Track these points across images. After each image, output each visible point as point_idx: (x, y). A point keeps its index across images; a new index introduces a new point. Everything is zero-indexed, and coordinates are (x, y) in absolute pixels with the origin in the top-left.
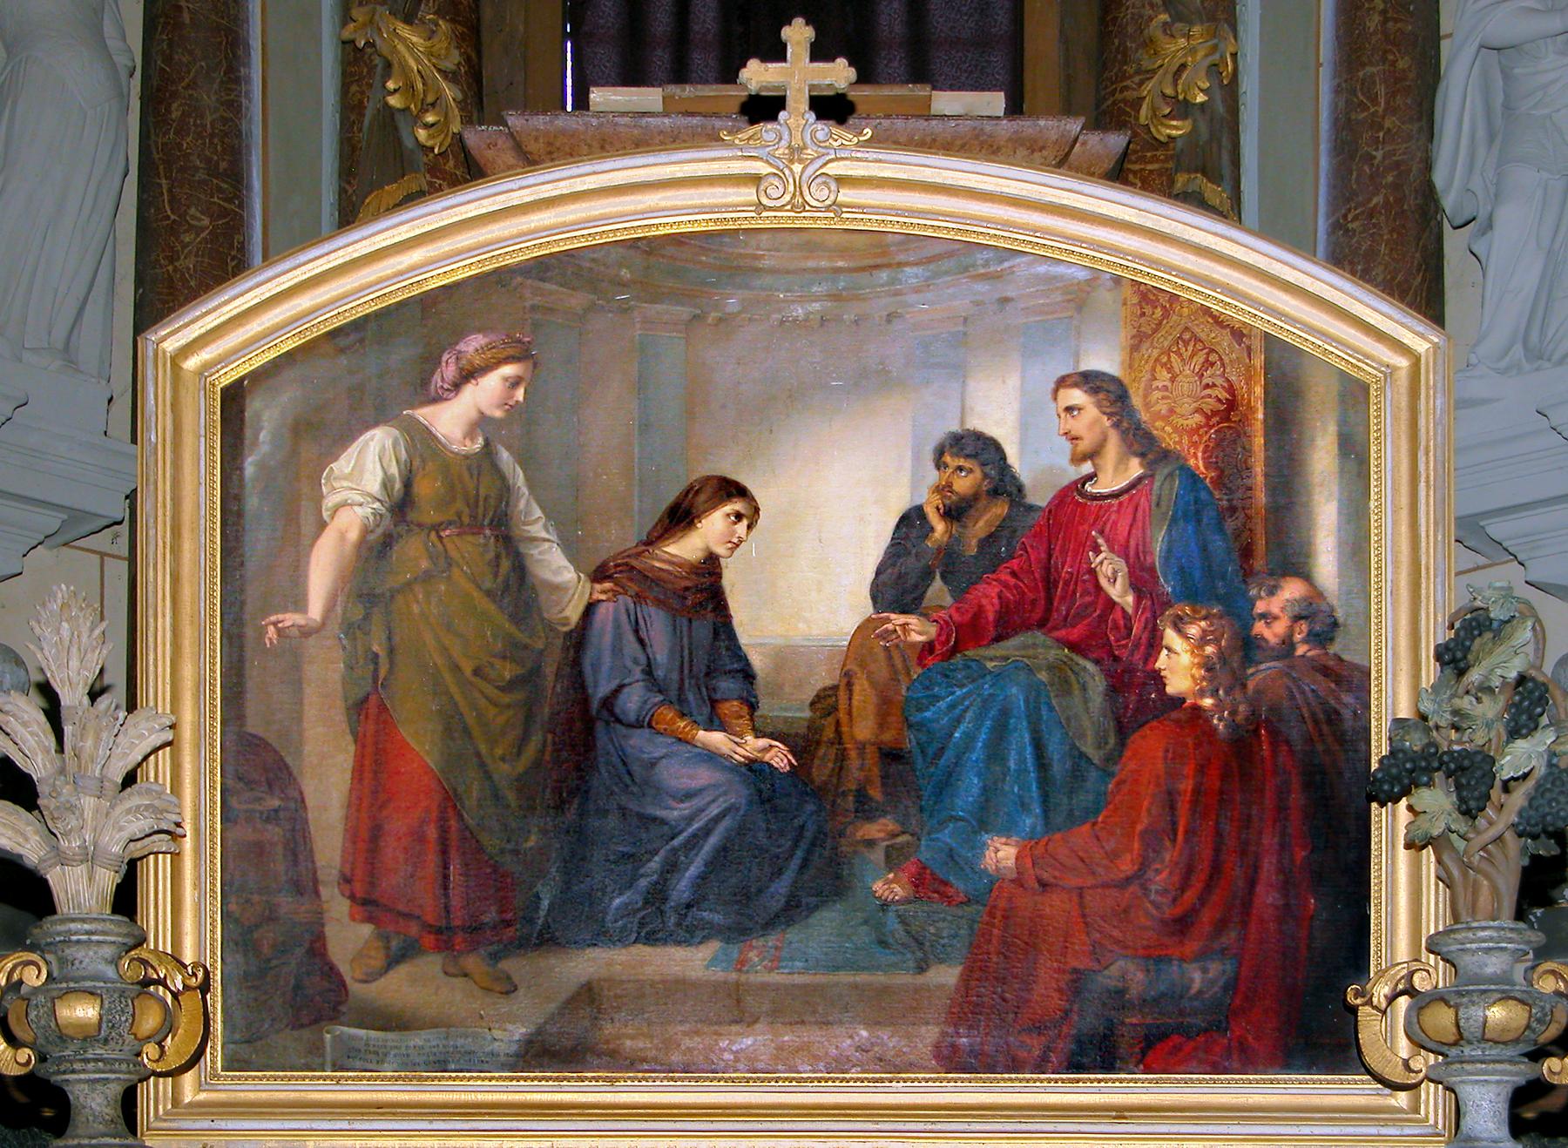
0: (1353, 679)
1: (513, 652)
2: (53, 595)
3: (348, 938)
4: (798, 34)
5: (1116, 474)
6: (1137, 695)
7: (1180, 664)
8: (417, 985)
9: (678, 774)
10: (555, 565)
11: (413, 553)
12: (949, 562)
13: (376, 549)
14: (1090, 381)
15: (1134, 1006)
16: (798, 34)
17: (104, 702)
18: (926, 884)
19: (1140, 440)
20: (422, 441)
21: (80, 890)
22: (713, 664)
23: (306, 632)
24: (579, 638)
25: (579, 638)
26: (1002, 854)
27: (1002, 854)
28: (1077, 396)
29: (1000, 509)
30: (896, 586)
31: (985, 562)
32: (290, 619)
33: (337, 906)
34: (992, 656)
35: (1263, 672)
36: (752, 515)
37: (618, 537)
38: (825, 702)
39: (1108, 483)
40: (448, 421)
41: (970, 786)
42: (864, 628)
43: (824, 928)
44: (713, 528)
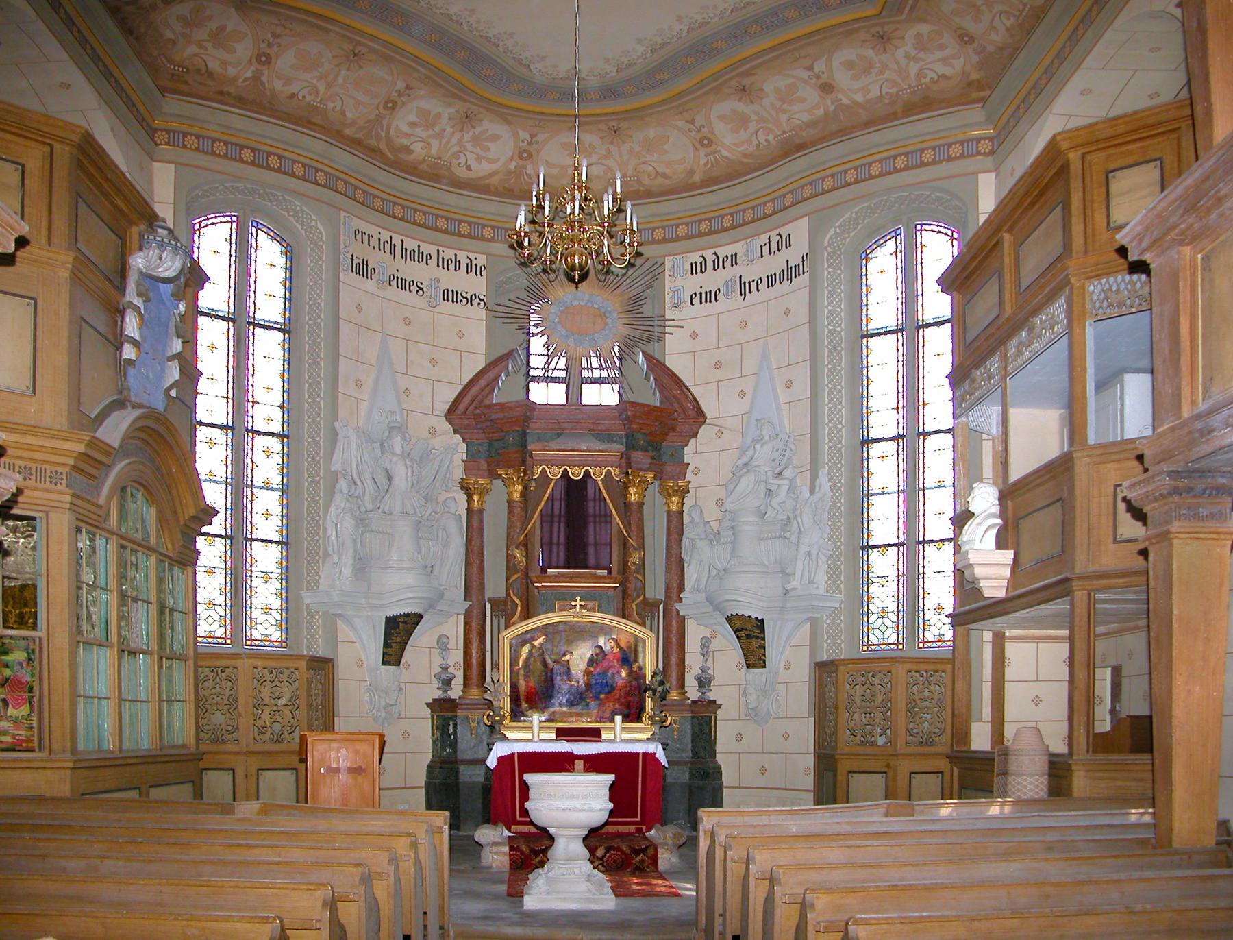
5: (616, 650)
13: (527, 660)
44: (567, 658)
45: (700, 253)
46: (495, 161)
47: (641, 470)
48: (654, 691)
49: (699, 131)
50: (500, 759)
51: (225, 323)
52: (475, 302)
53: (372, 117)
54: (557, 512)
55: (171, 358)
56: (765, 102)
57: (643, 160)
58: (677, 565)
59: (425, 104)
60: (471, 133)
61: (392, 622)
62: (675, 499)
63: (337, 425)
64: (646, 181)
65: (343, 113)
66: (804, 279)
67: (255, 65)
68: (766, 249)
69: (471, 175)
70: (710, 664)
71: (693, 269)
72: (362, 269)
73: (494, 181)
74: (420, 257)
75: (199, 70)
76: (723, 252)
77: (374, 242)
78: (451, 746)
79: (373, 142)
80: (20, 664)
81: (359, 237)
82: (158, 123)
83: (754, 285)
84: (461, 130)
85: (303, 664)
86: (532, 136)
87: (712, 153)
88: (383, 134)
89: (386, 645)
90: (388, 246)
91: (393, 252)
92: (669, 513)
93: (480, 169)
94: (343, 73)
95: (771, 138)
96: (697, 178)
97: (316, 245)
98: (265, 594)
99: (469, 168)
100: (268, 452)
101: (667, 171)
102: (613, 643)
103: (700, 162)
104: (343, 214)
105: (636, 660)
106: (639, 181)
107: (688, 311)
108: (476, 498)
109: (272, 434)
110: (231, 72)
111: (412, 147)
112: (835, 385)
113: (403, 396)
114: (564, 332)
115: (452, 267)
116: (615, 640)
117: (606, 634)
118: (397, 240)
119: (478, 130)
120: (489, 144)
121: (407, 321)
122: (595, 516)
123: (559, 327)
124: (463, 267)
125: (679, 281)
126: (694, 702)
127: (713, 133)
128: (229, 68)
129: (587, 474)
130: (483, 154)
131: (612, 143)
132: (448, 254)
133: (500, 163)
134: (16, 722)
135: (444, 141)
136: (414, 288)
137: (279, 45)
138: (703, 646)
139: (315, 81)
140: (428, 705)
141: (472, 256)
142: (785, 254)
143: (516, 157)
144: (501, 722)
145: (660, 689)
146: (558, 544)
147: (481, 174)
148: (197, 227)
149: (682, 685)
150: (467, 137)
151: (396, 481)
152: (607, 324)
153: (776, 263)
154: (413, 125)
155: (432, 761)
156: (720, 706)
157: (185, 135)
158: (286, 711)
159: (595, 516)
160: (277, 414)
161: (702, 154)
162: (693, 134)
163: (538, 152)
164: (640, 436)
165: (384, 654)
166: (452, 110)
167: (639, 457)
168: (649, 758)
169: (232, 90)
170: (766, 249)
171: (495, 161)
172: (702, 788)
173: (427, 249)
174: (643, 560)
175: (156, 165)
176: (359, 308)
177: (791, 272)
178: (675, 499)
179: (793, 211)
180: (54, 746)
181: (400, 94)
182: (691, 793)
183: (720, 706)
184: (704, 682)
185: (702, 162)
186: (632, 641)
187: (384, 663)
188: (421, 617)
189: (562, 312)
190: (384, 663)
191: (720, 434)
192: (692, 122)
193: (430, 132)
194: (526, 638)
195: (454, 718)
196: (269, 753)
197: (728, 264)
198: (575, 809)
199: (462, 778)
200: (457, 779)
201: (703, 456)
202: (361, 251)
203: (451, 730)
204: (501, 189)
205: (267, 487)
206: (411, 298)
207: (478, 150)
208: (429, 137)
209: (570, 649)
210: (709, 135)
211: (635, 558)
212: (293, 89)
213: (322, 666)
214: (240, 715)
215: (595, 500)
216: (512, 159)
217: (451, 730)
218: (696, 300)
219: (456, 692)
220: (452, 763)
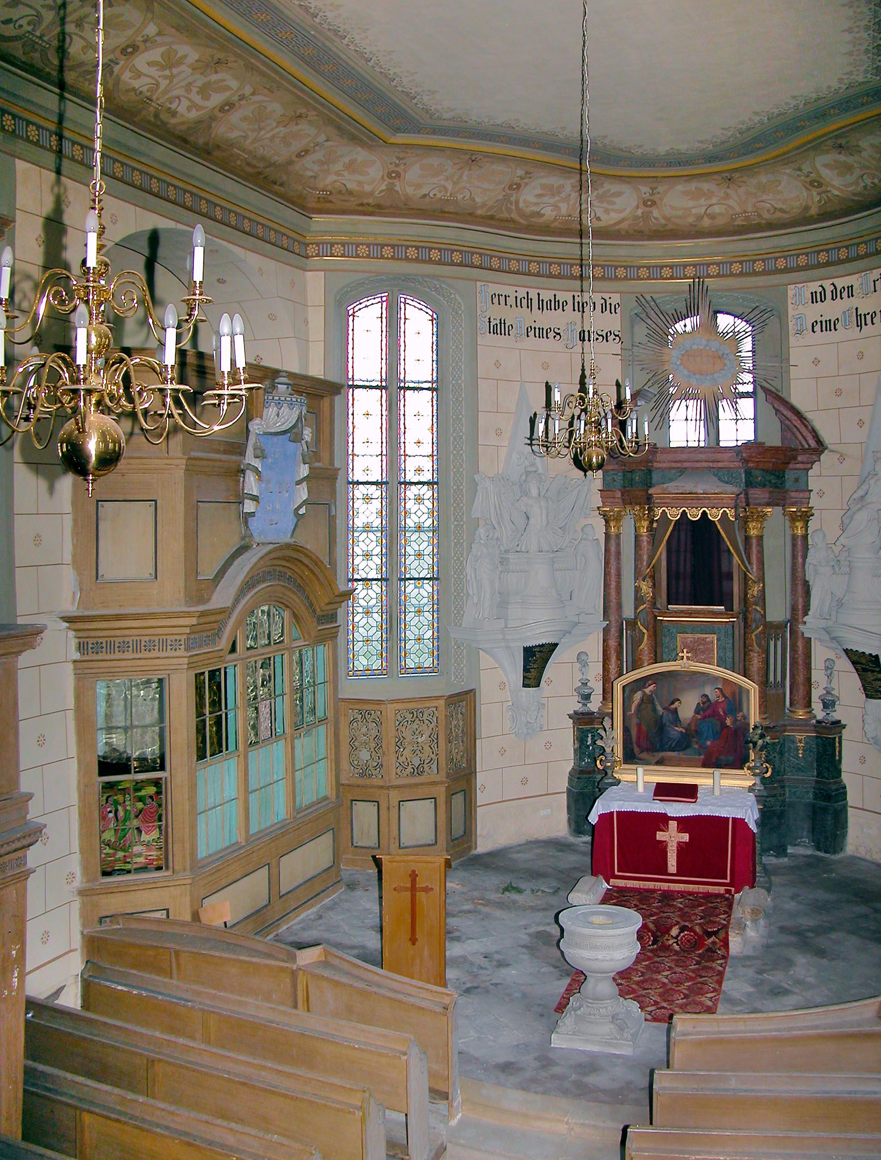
3: (636, 750)
4: (685, 837)
6: (724, 726)
7: (728, 722)
8: (644, 755)
9: (673, 732)
10: (659, 708)
11: (644, 706)
13: (639, 705)
16: (685, 837)
18: (700, 746)
19: (724, 696)
21: (608, 750)
22: (677, 720)
24: (661, 716)
25: (661, 716)
26: (709, 743)
27: (709, 743)
30: (697, 711)
31: (706, 708)
33: (635, 746)
34: (707, 720)
35: (738, 723)
38: (689, 725)
40: (647, 691)
41: (705, 735)
43: (688, 751)
44: (677, 703)
45: (820, 283)
46: (621, 211)
47: (759, 504)
48: (755, 744)
49: (807, 176)
50: (601, 816)
51: (379, 391)
52: (610, 338)
53: (500, 197)
55: (299, 483)
56: (863, 154)
57: (759, 199)
58: (802, 591)
59: (545, 181)
61: (529, 652)
62: (799, 524)
63: (476, 477)
64: (766, 215)
65: (473, 200)
67: (388, 180)
70: (834, 684)
71: (815, 298)
72: (499, 328)
73: (624, 226)
74: (556, 305)
75: (340, 192)
76: (840, 283)
79: (505, 215)
80: (151, 797)
81: (496, 300)
82: (309, 239)
83: (869, 317)
85: (442, 702)
86: (653, 189)
87: (824, 192)
88: (513, 207)
89: (526, 670)
90: (524, 302)
91: (530, 306)
92: (794, 537)
94: (466, 173)
96: (813, 211)
98: (419, 627)
99: (598, 219)
100: (419, 499)
101: (784, 207)
103: (814, 201)
105: (741, 710)
106: (759, 215)
108: (612, 524)
109: (423, 483)
110: (368, 188)
114: (686, 372)
118: (533, 295)
120: (614, 199)
123: (681, 368)
124: (598, 307)
126: (818, 722)
127: (821, 177)
128: (365, 186)
131: (728, 187)
134: (148, 845)
135: (571, 203)
137: (405, 164)
138: (827, 668)
139: (442, 182)
140: (570, 717)
141: (606, 296)
144: (612, 767)
145: (760, 742)
148: (351, 312)
149: (808, 704)
151: (532, 521)
152: (725, 365)
154: (539, 196)
156: (844, 727)
157: (332, 245)
158: (426, 748)
160: (427, 464)
161: (814, 193)
163: (661, 199)
164: (757, 473)
165: (524, 677)
166: (573, 181)
167: (757, 494)
168: (739, 823)
169: (370, 201)
171: (621, 211)
172: (825, 810)
173: (561, 296)
174: (763, 591)
175: (309, 274)
176: (497, 365)
178: (799, 524)
180: (177, 868)
181: (522, 178)
182: (814, 813)
183: (844, 727)
187: (525, 686)
188: (556, 645)
189: (683, 355)
190: (525, 686)
192: (800, 170)
193: (557, 198)
196: (410, 786)
197: (845, 295)
201: (824, 483)
202: (497, 312)
204: (631, 232)
205: (419, 528)
206: (550, 344)
207: (605, 205)
208: (558, 201)
210: (817, 179)
211: (755, 590)
212: (425, 191)
213: (464, 702)
214: (384, 753)
216: (637, 207)
218: (817, 328)
219: (595, 705)
220: (589, 773)
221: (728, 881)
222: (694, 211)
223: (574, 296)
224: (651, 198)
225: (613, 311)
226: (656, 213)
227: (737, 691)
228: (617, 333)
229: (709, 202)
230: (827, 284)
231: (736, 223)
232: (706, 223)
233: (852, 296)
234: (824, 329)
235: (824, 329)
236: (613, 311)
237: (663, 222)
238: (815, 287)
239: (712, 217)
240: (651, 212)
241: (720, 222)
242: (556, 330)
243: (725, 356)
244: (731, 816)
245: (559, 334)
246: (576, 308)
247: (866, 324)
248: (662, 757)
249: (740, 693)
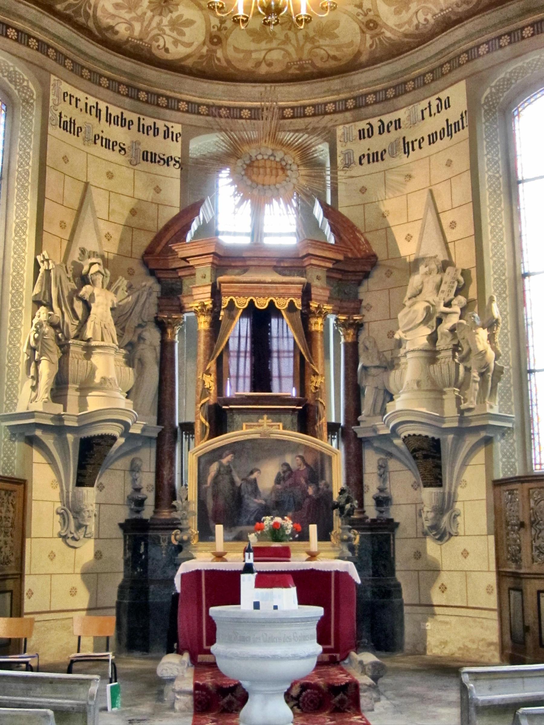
0: (331, 494)
1: (233, 490)
2: (165, 554)
5: (303, 468)
9: (251, 505)
12: (284, 479)
13: (216, 477)
14: (300, 457)
15: (138, 512)
17: (185, 497)
20: (221, 465)
22: (255, 491)
23: (207, 487)
24: (240, 488)
28: (298, 458)
29: (289, 472)
31: (286, 476)
32: (205, 486)
35: (320, 492)
36: (260, 473)
37: (245, 476)
39: (301, 469)
40: (225, 461)
42: (273, 487)
44: (255, 475)
54: (242, 348)
60: (168, 18)
64: (319, 64)
66: (464, 133)
68: (426, 113)
69: (169, 57)
71: (362, 135)
73: (189, 63)
76: (387, 119)
77: (81, 105)
78: (141, 567)
81: (67, 98)
83: (416, 144)
84: (160, 14)
87: (377, 35)
90: (94, 111)
93: (177, 52)
95: (429, 17)
96: (364, 58)
97: (28, 103)
99: (167, 50)
101: (336, 53)
102: (299, 461)
104: (53, 77)
105: (323, 478)
107: (357, 170)
111: (117, 28)
112: (496, 224)
113: (104, 240)
115: (151, 132)
116: (302, 458)
117: (293, 452)
118: (102, 106)
119: (175, 15)
121: (110, 175)
122: (278, 352)
125: (350, 146)
126: (373, 521)
127: (378, 16)
129: (272, 303)
130: (179, 38)
132: (148, 122)
133: (194, 48)
135: (145, 23)
136: (117, 148)
141: (169, 125)
142: (445, 114)
143: (208, 42)
146: (244, 377)
147: (177, 57)
150: (166, 21)
153: (436, 123)
155: (124, 581)
159: (278, 352)
161: (368, 36)
162: (360, 17)
170: (426, 113)
171: (190, 45)
176: (65, 159)
177: (450, 129)
179: (452, 77)
184: (382, 502)
185: (368, 45)
186: (319, 458)
191: (389, 274)
193: (133, 15)
194: (215, 454)
195: (145, 538)
197: (392, 128)
198: (275, 658)
199: (151, 599)
200: (147, 599)
202: (69, 111)
203: (142, 550)
207: (175, 34)
209: (257, 466)
215: (278, 337)
216: (204, 43)
217: (142, 550)
218: (365, 161)
219: (147, 513)
221: (332, 646)
222: (254, 55)
223: (139, 119)
224: (218, 33)
225: (174, 139)
226: (219, 54)
227: (319, 458)
228: (177, 159)
229: (269, 46)
230: (375, 122)
231: (290, 72)
232: (263, 70)
233: (400, 127)
234: (371, 160)
235: (371, 160)
236: (174, 139)
237: (224, 64)
238: (363, 125)
239: (270, 65)
240: (215, 52)
241: (277, 69)
242: (122, 145)
243: (288, 167)
244: (333, 569)
245: (124, 149)
246: (141, 130)
247: (413, 150)
248: (241, 532)
249: (322, 461)
